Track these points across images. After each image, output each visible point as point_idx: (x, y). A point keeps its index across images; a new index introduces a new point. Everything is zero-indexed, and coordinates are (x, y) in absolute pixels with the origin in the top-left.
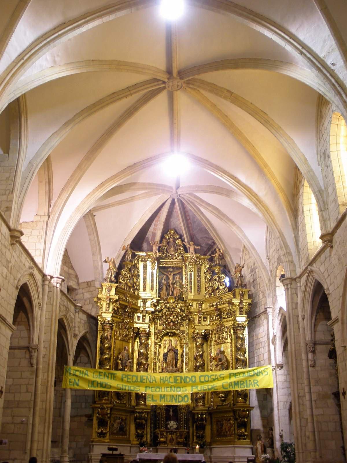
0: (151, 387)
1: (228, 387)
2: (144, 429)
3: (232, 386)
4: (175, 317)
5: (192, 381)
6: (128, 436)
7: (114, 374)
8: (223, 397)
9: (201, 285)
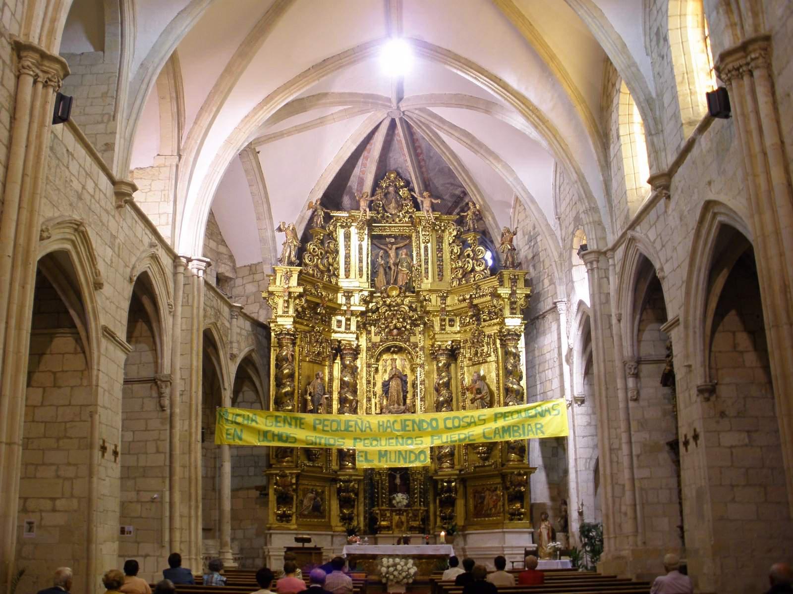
0: (363, 438)
1: (493, 436)
2: (353, 506)
3: (499, 433)
4: (401, 320)
5: (432, 427)
6: (327, 520)
7: (301, 419)
8: (484, 453)
9: (444, 266)
